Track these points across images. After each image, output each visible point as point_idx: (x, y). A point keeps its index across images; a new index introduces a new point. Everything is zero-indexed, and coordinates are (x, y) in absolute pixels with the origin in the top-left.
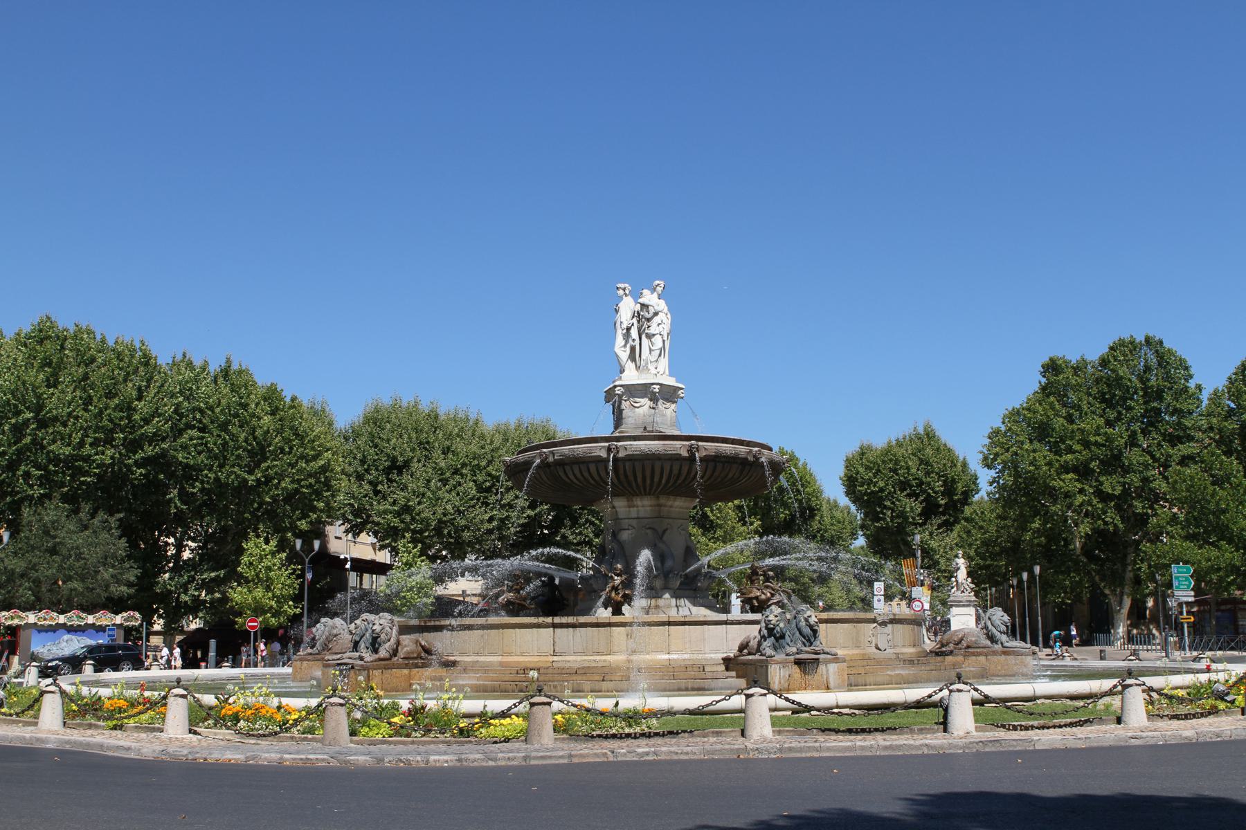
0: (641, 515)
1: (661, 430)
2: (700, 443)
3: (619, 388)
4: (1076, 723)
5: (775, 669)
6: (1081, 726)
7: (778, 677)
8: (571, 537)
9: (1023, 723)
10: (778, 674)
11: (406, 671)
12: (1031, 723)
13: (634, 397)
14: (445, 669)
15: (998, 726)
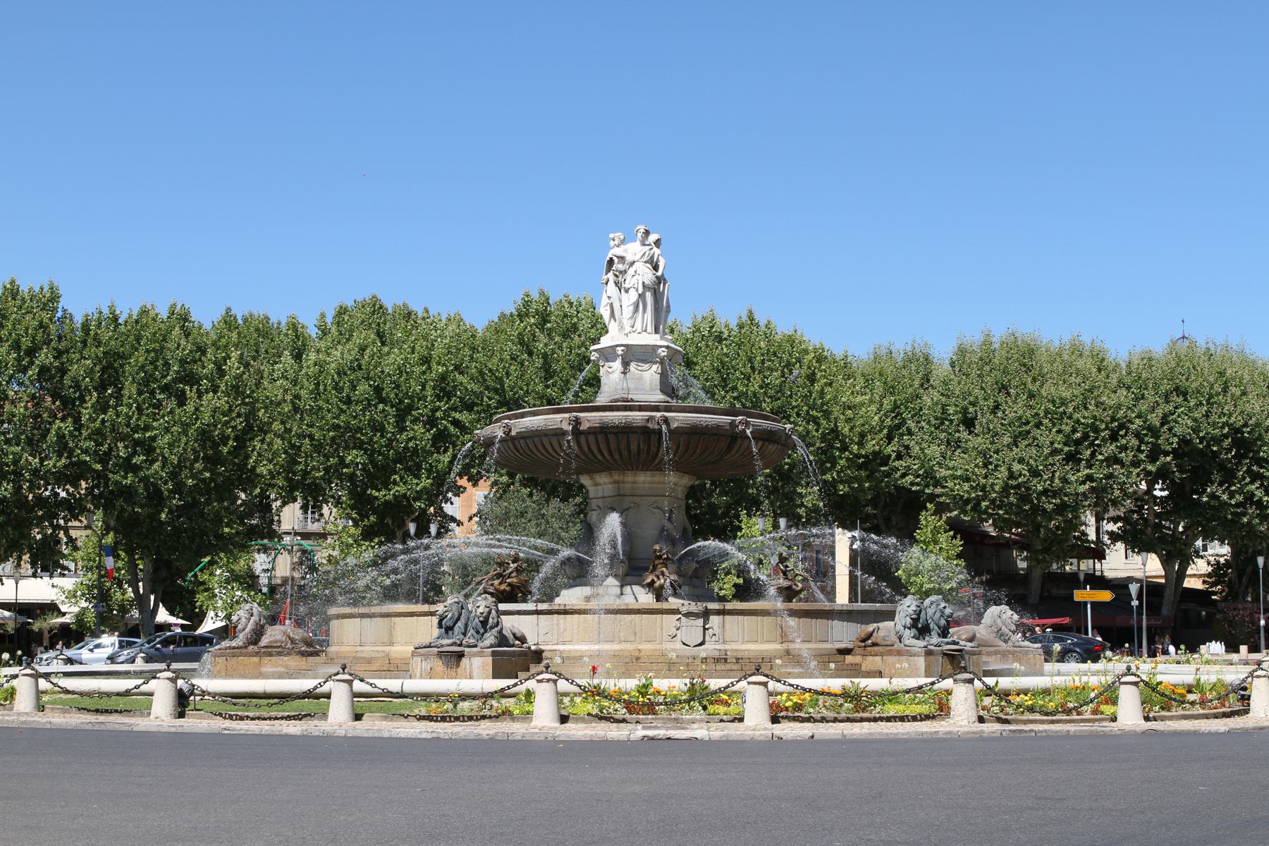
0: (606, 494)
1: (635, 397)
2: (581, 415)
3: (664, 349)
4: (294, 716)
5: (417, 661)
6: (300, 719)
7: (419, 670)
8: (1225, 497)
9: (239, 713)
10: (419, 666)
11: (256, 659)
12: (246, 714)
13: (608, 361)
14: (304, 658)
15: (215, 715)
